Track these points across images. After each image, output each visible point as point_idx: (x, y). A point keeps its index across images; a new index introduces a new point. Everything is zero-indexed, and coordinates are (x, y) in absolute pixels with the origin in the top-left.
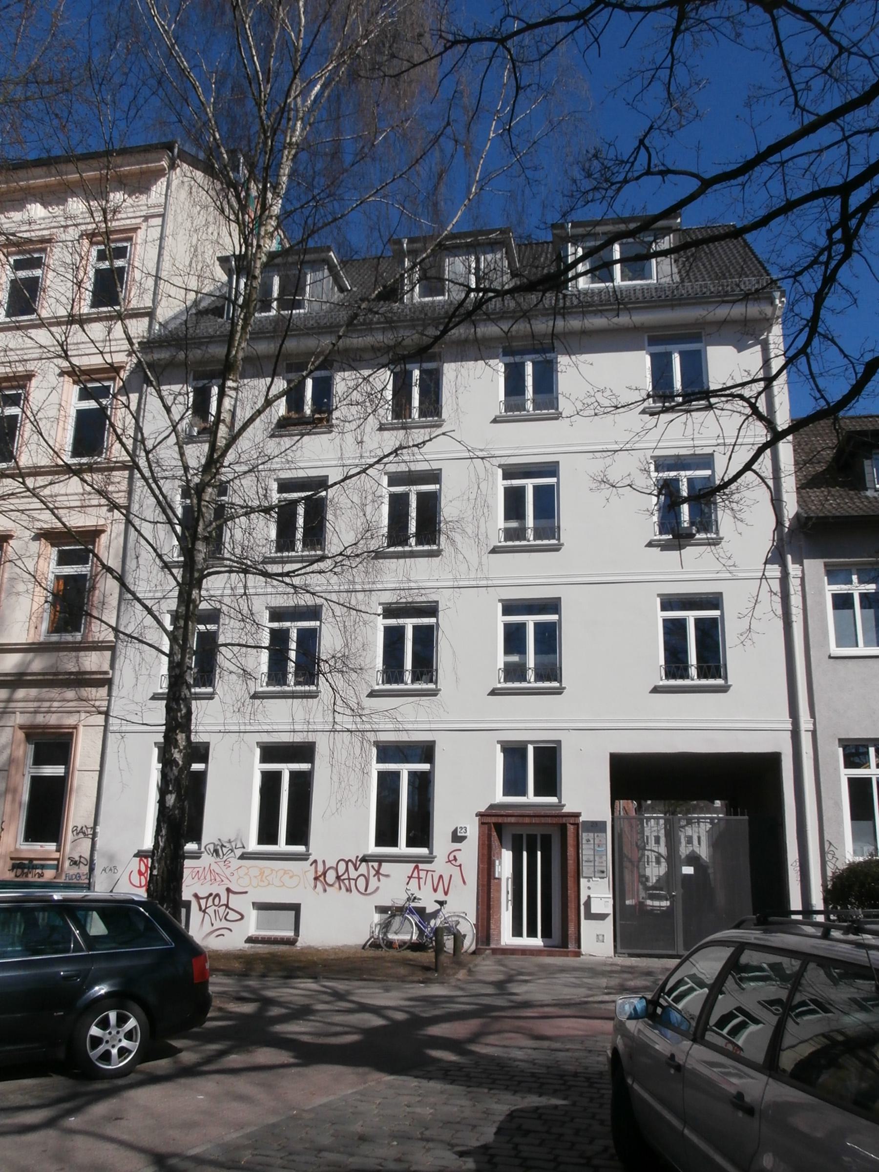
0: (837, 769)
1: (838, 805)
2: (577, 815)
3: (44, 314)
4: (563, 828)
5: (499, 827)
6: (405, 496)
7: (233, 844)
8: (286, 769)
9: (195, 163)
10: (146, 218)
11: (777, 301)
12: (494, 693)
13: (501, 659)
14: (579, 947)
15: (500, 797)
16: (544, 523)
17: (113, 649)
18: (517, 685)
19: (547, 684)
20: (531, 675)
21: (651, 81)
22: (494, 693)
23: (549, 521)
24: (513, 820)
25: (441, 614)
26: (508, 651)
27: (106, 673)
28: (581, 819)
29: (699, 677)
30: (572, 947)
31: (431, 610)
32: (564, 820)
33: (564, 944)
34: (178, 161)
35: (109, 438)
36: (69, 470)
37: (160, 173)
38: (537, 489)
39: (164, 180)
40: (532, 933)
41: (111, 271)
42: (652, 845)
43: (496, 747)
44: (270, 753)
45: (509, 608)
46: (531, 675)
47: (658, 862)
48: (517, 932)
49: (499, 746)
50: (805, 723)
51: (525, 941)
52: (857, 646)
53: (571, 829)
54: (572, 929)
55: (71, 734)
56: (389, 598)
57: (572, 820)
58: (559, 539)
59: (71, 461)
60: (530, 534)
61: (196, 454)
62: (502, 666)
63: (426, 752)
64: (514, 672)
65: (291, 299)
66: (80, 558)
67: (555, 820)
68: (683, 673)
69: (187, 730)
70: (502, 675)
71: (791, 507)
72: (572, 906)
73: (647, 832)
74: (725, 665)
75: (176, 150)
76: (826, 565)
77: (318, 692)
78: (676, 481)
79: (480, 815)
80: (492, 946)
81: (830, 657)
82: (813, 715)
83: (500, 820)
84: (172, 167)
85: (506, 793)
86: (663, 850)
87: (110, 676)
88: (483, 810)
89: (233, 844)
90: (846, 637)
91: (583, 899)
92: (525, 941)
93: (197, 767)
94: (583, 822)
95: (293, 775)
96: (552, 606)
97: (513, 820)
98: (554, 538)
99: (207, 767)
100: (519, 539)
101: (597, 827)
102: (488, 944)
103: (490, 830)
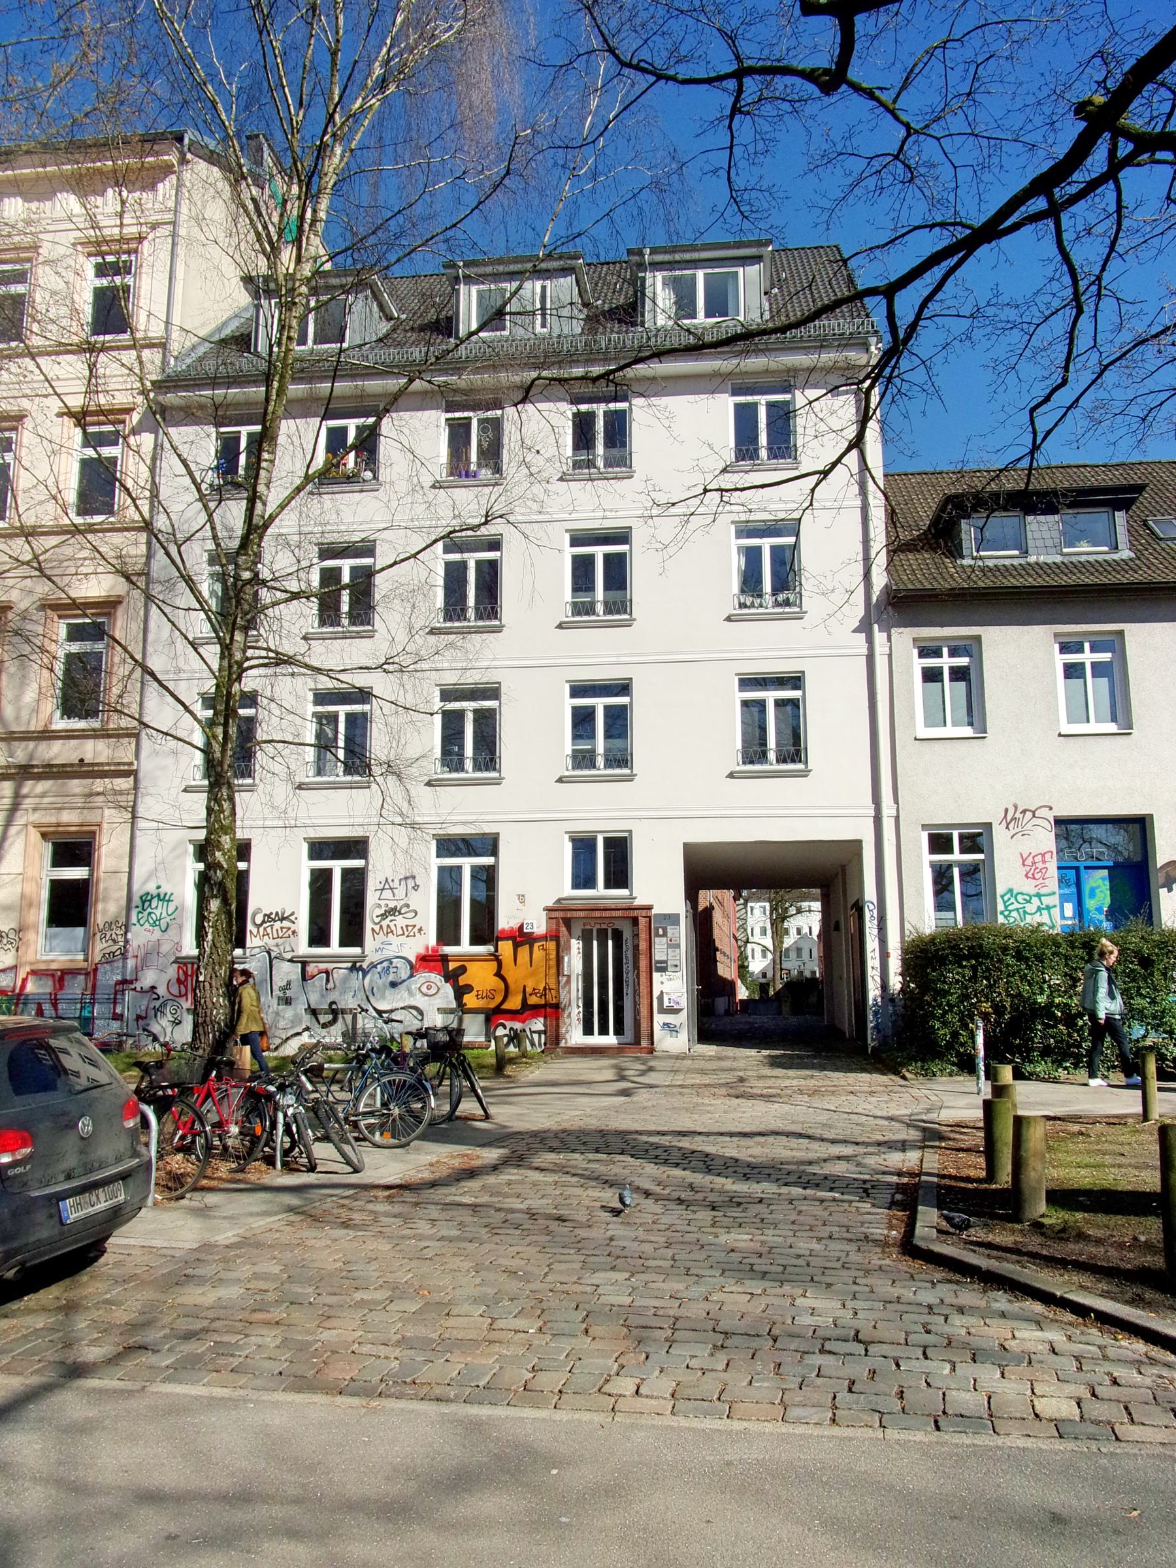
0: (920, 856)
1: (920, 893)
2: (649, 908)
3: (36, 341)
4: (635, 921)
5: (568, 922)
6: (463, 565)
7: (282, 948)
8: (337, 866)
9: (212, 158)
10: (154, 227)
11: (873, 348)
12: (731, 775)
13: (568, 748)
14: (652, 1043)
15: (568, 891)
16: (615, 595)
17: (137, 736)
18: (586, 772)
19: (618, 771)
20: (600, 761)
21: (709, 81)
22: (731, 775)
23: (619, 592)
24: (582, 914)
25: (503, 697)
26: (576, 737)
27: (131, 764)
28: (654, 912)
29: (778, 761)
30: (644, 1043)
31: (493, 692)
32: (635, 913)
33: (637, 1041)
34: (189, 156)
35: (120, 497)
36: (75, 530)
37: (167, 170)
38: (607, 557)
39: (173, 178)
40: (604, 1031)
41: (114, 289)
42: (757, 937)
43: (563, 839)
44: (319, 849)
45: (578, 690)
46: (600, 761)
47: (764, 956)
48: (588, 1031)
49: (567, 837)
50: (888, 809)
51: (596, 1040)
52: (1088, 721)
53: (642, 922)
54: (644, 1025)
55: (94, 833)
56: (450, 678)
57: (644, 913)
58: (631, 614)
59: (79, 520)
60: (600, 608)
61: (234, 513)
62: (570, 753)
63: (490, 845)
64: (583, 759)
65: (333, 331)
66: (97, 632)
67: (626, 914)
68: (762, 757)
69: (230, 829)
70: (570, 761)
71: (880, 580)
72: (644, 1002)
73: (751, 922)
74: (806, 749)
75: (186, 141)
76: (1056, 635)
77: (254, 785)
78: (338, 570)
79: (549, 910)
80: (562, 1044)
81: (1060, 735)
82: (896, 801)
83: (569, 915)
84: (183, 161)
85: (576, 886)
86: (768, 942)
87: (135, 767)
88: (550, 904)
89: (282, 948)
90: (936, 716)
91: (656, 994)
92: (596, 1040)
93: (242, 865)
94: (656, 915)
95: (346, 872)
96: (795, 681)
97: (582, 914)
98: (625, 612)
99: (497, 861)
100: (587, 614)
101: (673, 919)
102: (558, 1043)
103: (558, 925)
